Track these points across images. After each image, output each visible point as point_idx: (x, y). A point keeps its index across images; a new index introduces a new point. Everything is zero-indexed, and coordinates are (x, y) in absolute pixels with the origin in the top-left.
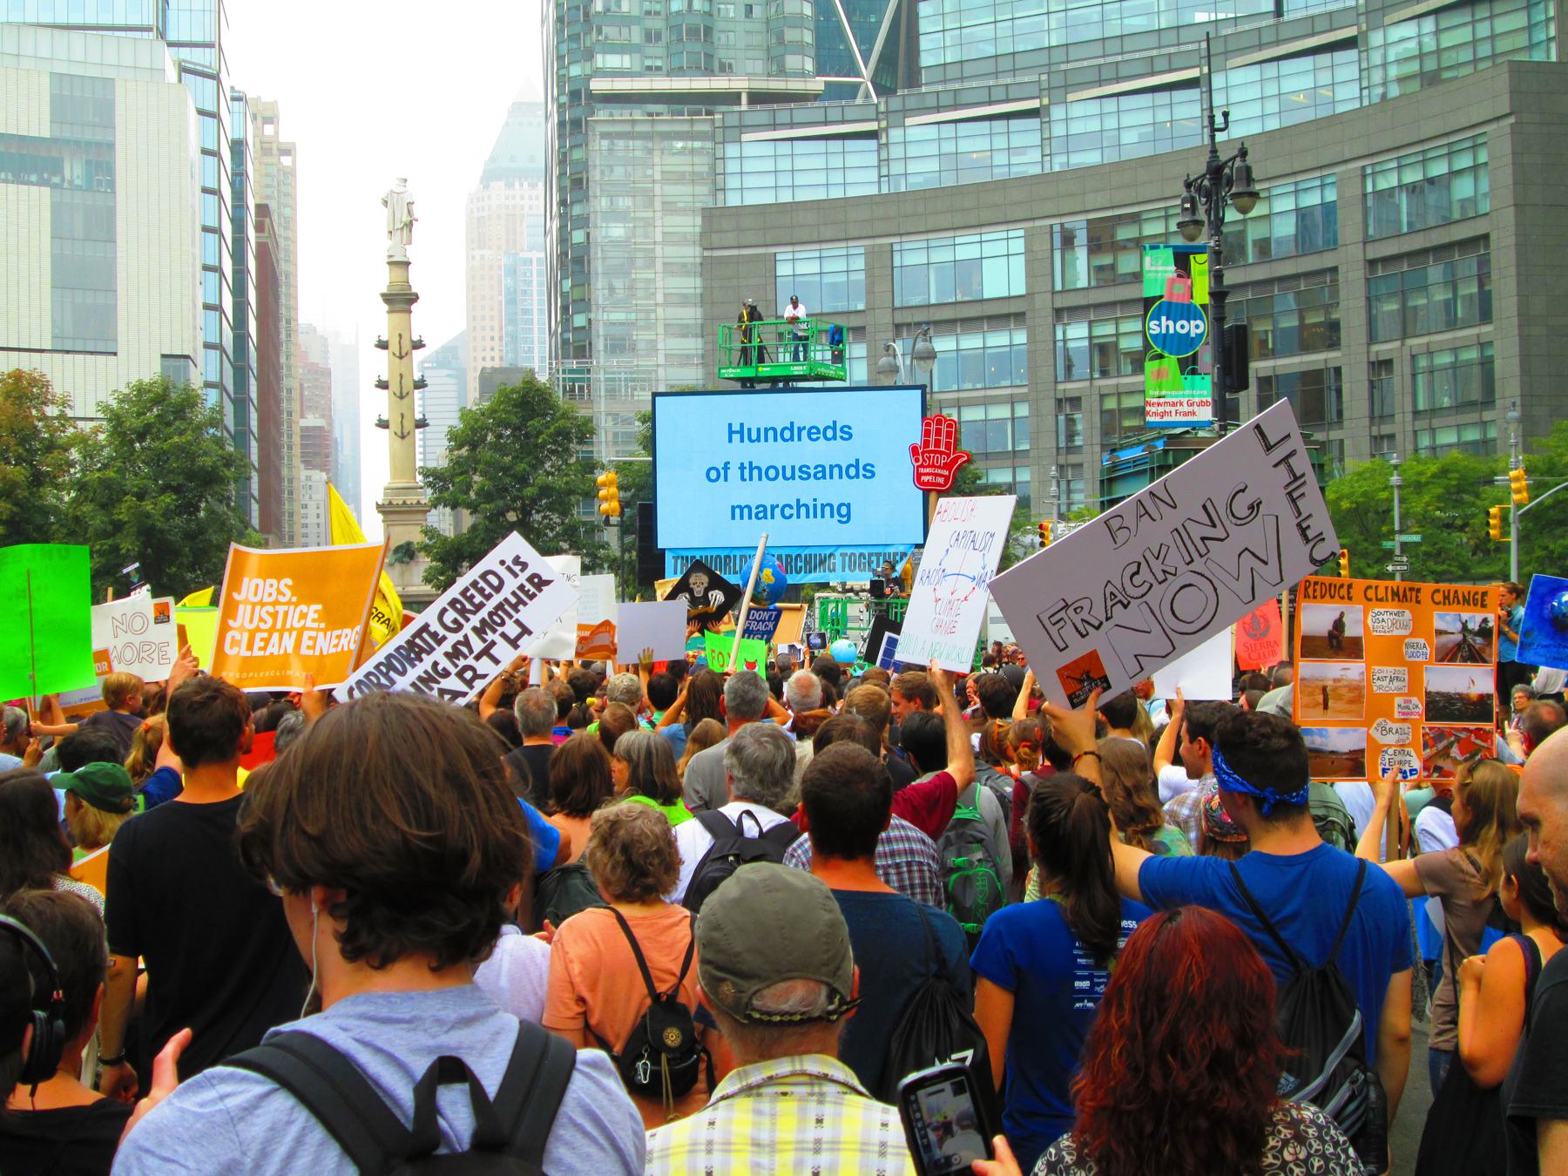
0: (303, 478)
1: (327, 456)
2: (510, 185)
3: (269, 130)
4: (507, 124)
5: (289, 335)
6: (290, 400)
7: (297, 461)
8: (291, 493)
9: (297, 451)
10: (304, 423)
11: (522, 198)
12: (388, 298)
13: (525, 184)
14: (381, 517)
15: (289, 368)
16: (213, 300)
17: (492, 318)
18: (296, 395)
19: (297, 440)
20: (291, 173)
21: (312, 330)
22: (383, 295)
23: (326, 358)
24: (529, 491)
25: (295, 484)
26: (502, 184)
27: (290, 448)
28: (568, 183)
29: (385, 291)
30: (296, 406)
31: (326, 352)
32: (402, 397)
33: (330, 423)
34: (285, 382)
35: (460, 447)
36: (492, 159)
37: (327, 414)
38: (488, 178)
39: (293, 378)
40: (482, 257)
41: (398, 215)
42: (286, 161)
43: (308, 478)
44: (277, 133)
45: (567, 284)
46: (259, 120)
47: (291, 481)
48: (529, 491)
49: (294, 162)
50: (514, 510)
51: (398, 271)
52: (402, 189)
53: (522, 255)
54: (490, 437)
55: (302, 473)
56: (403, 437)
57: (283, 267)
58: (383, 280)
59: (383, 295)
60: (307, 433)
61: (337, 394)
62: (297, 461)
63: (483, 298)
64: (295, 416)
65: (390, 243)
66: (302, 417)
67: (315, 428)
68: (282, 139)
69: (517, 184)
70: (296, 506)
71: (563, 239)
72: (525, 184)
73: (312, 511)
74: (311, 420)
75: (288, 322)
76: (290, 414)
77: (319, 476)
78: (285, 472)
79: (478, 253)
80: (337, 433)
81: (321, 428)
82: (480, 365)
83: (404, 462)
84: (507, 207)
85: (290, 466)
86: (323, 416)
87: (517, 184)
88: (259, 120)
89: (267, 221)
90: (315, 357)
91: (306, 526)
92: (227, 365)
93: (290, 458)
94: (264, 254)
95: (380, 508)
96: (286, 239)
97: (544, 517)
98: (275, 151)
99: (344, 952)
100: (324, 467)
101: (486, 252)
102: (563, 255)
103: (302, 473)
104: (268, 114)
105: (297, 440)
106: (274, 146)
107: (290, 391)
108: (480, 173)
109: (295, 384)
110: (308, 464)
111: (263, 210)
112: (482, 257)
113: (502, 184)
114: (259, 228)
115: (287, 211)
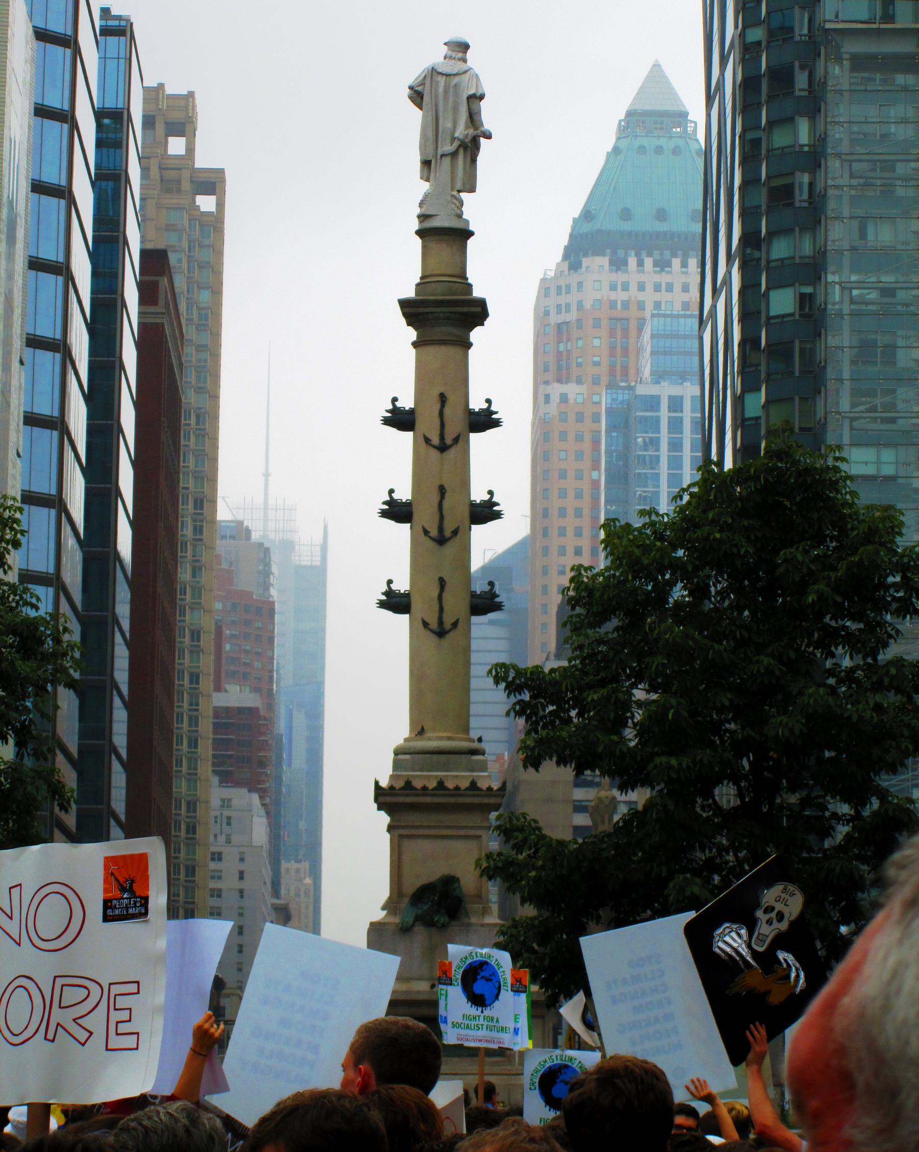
0: (215, 802)
1: (262, 764)
2: (618, 264)
3: (176, 146)
4: (616, 150)
5: (198, 530)
6: (196, 651)
7: (205, 769)
8: (191, 829)
9: (206, 749)
10: (220, 700)
11: (641, 287)
12: (413, 311)
13: (648, 262)
14: (384, 819)
15: (197, 591)
16: (46, 407)
17: (578, 513)
18: (207, 641)
19: (206, 728)
20: (213, 225)
21: (240, 531)
22: (405, 305)
23: (266, 586)
24: (783, 724)
25: (200, 811)
26: (604, 261)
27: (193, 743)
28: (761, 198)
29: (410, 293)
30: (207, 662)
31: (267, 573)
32: (441, 541)
33: (270, 707)
34: (190, 619)
35: (601, 618)
36: (587, 215)
37: (264, 684)
38: (578, 249)
39: (204, 613)
40: (564, 399)
41: (446, 124)
42: (206, 203)
43: (226, 803)
44: (190, 149)
45: (757, 402)
46: (160, 128)
47: (192, 806)
48: (783, 724)
49: (220, 205)
50: (735, 778)
51: (443, 251)
52: (459, 67)
53: (641, 390)
54: (679, 593)
55: (216, 793)
56: (441, 633)
57: (190, 398)
58: (404, 268)
59: (405, 305)
60: (227, 720)
61: (283, 652)
62: (205, 769)
63: (563, 474)
64: (206, 684)
65: (425, 186)
66: (218, 688)
67: (240, 710)
68: (202, 161)
69: (632, 261)
70: (200, 854)
71: (751, 310)
72: (648, 262)
73: (229, 866)
74: (235, 696)
75: (199, 503)
76: (195, 678)
77: (247, 800)
78: (181, 788)
79: (556, 390)
80: (281, 726)
81: (252, 712)
82: (570, 560)
83: (437, 693)
84: (613, 304)
85: (192, 778)
86: (256, 690)
87: (632, 261)
88: (160, 128)
89: (164, 281)
90: (245, 582)
91: (217, 893)
92: (70, 542)
93: (193, 761)
94: (152, 342)
95: (385, 798)
96: (201, 348)
97: (806, 802)
98: (186, 185)
99: (271, 612)
100: (254, 785)
101: (572, 390)
102: (749, 342)
103: (216, 793)
104: (176, 116)
105: (206, 728)
106: (186, 175)
107: (196, 635)
108: (565, 241)
109: (207, 623)
110: (227, 779)
111: (155, 262)
112: (564, 399)
113: (604, 261)
114: (147, 293)
115: (204, 297)
